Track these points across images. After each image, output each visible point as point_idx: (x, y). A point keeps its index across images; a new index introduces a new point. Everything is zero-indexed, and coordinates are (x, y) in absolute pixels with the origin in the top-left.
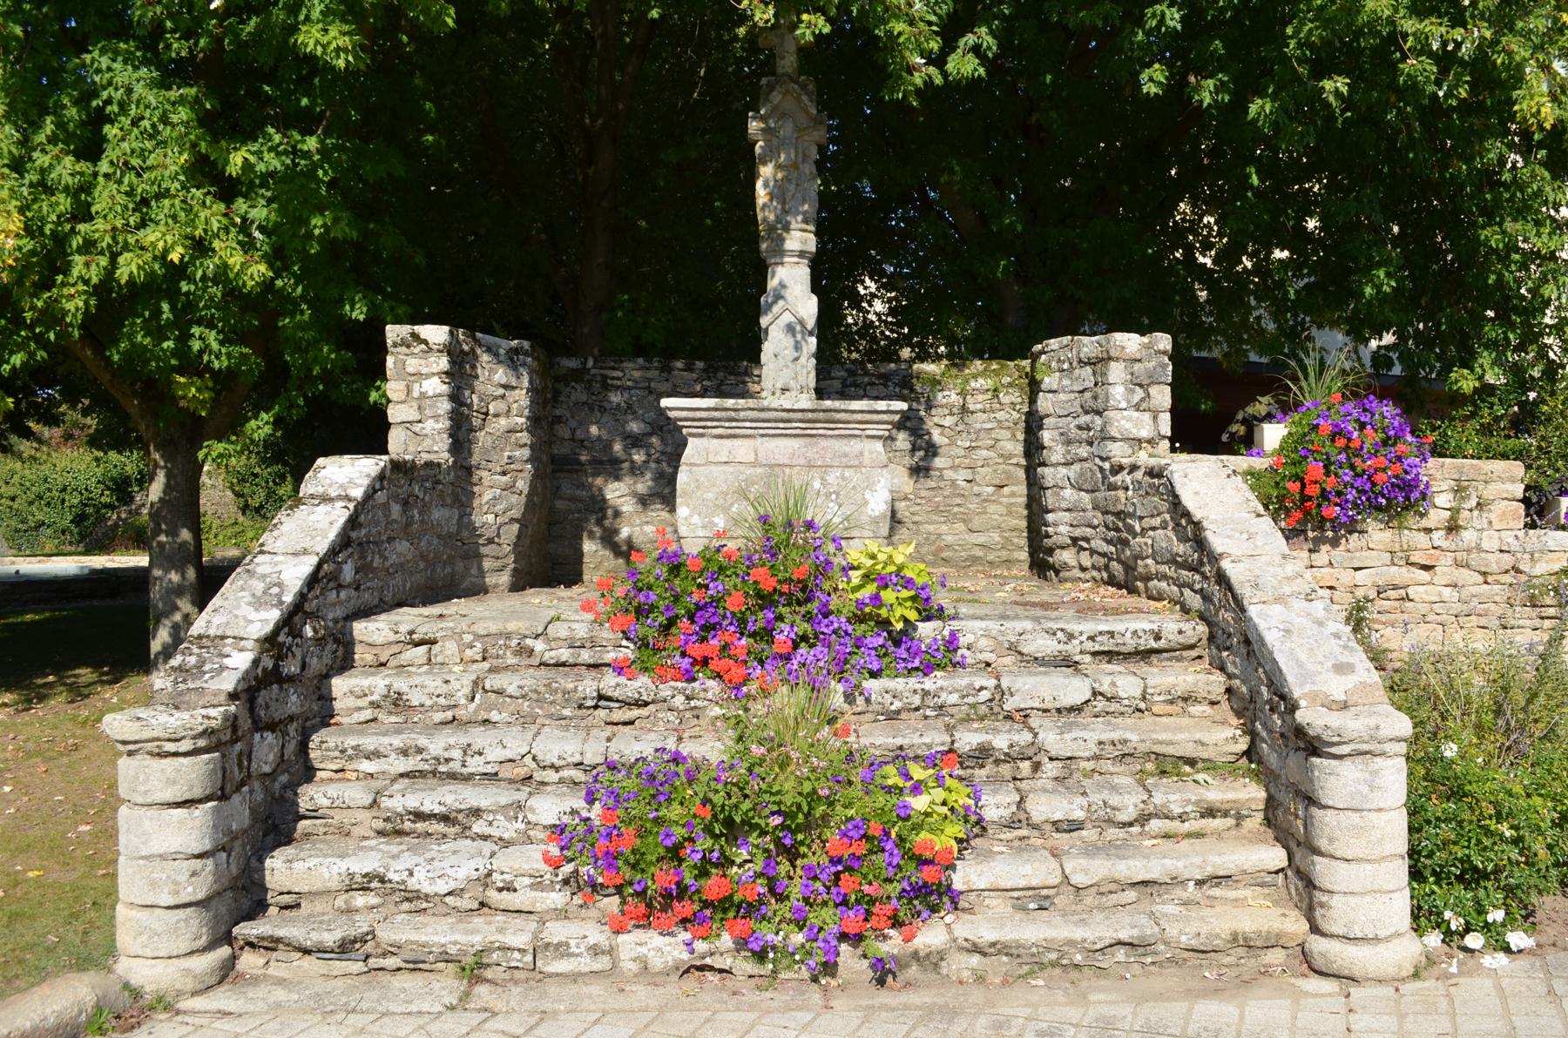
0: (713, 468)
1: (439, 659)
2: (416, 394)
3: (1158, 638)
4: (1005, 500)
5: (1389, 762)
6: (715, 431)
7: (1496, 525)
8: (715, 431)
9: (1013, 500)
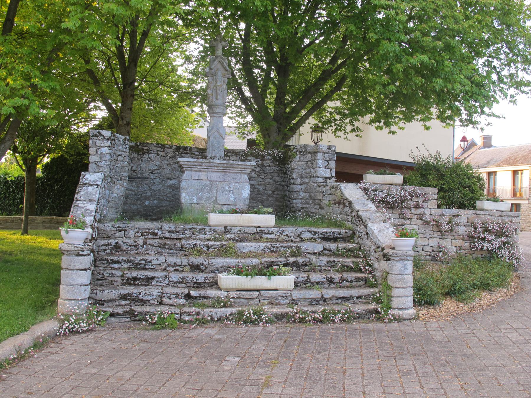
0: (193, 181)
1: (128, 236)
2: (99, 153)
3: (340, 234)
4: (274, 196)
5: (409, 262)
6: (194, 169)
7: (429, 207)
8: (196, 169)
9: (278, 196)
